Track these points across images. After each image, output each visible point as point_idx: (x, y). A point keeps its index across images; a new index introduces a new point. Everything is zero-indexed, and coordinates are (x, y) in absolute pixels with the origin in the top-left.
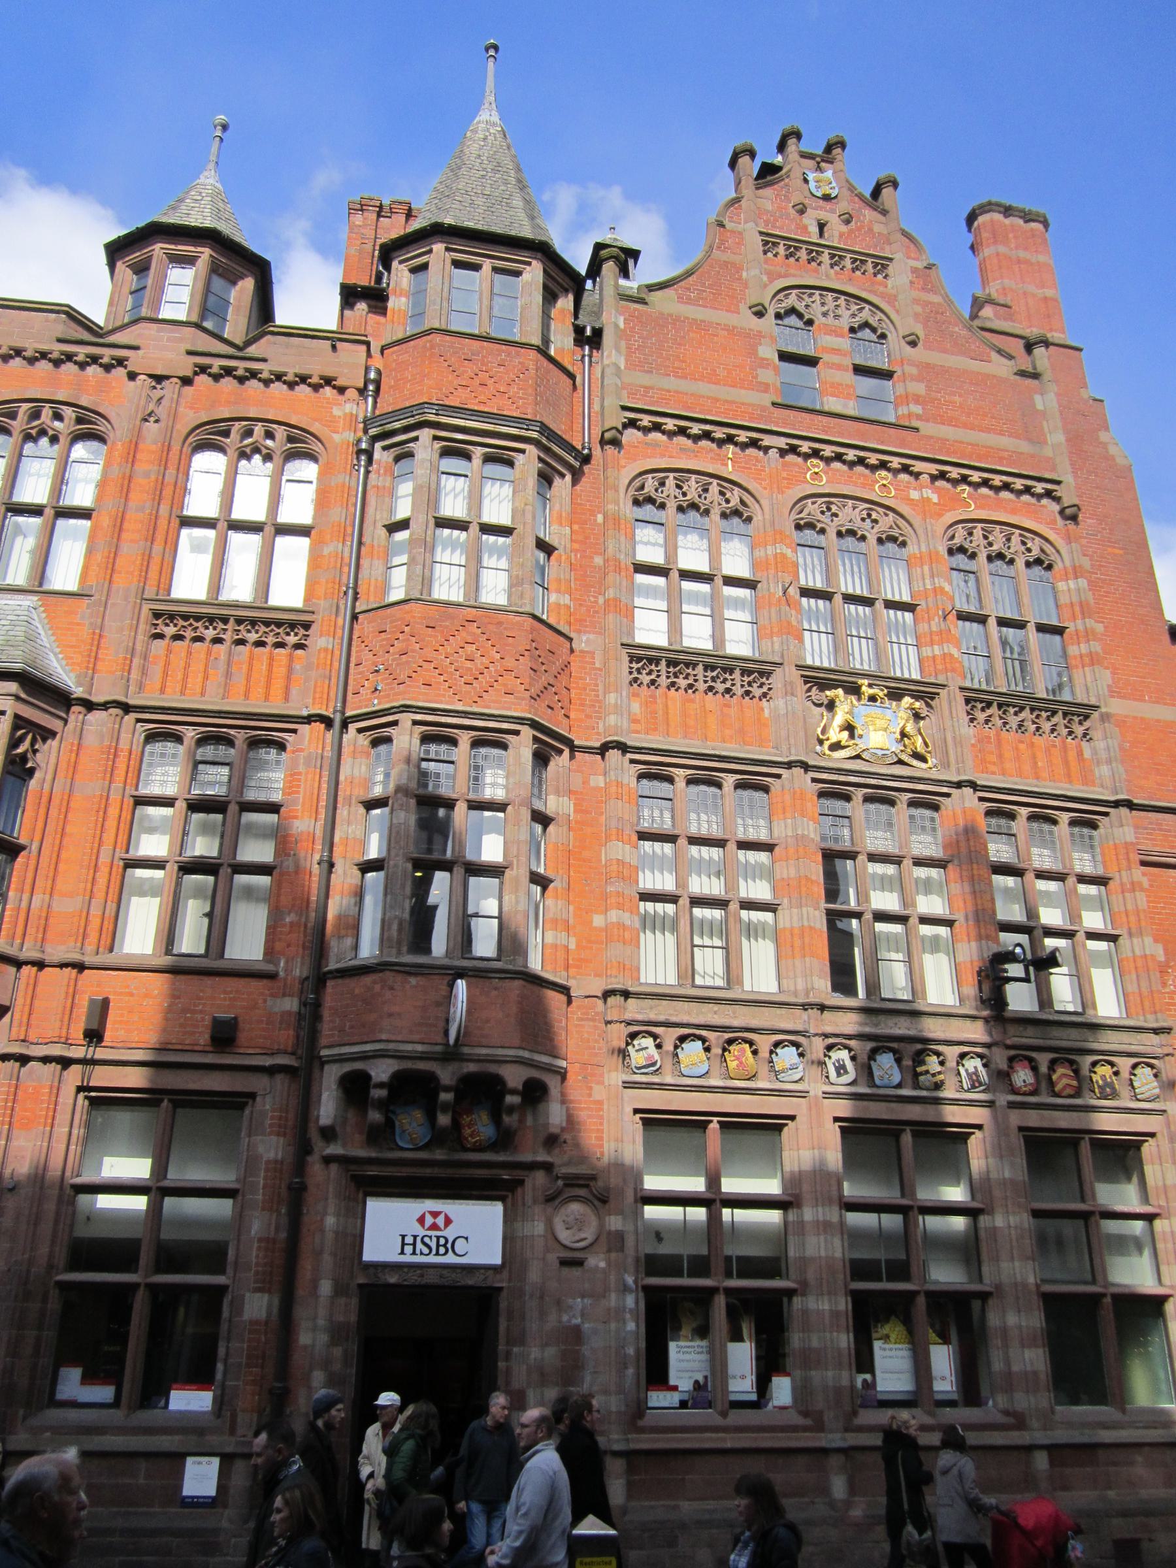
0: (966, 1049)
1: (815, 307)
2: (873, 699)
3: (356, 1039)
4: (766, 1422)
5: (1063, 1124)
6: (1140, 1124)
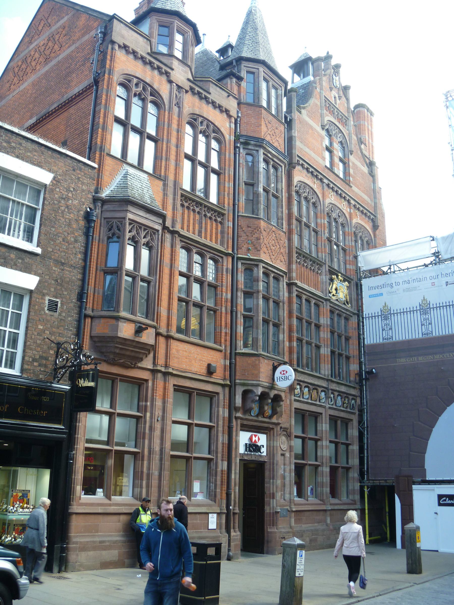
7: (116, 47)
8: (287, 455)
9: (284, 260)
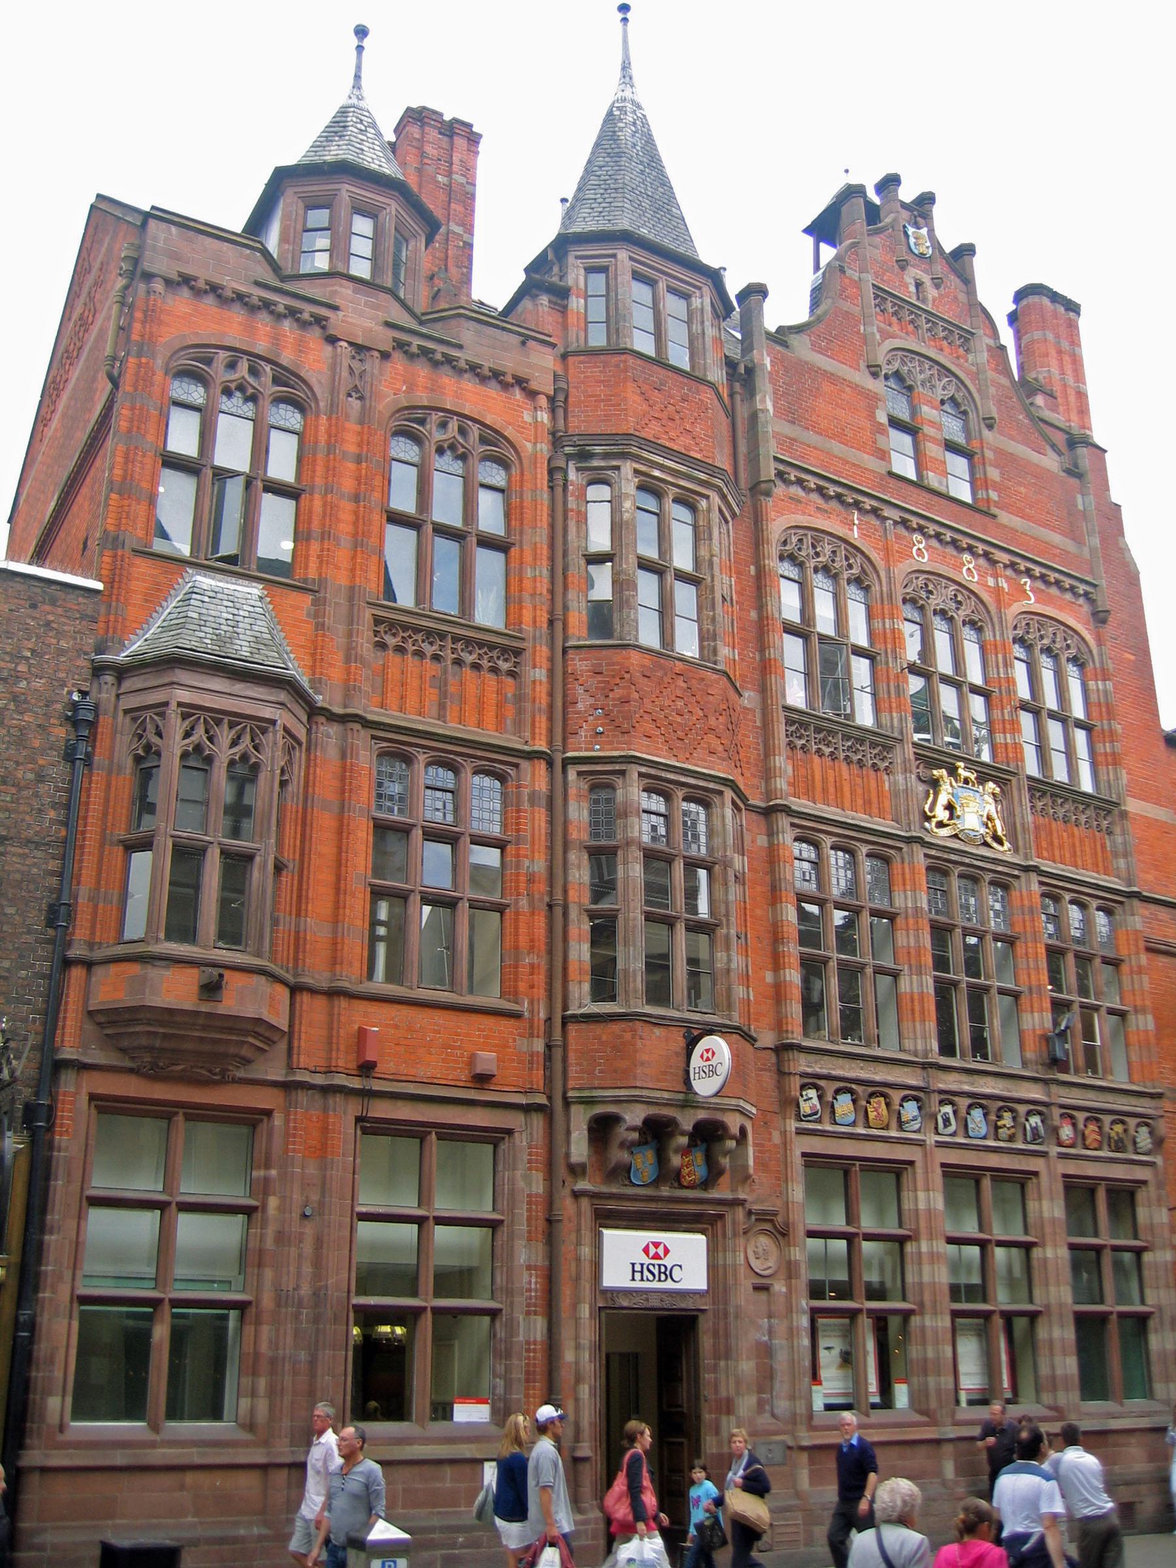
0: (1032, 1107)
1: (918, 374)
2: (966, 781)
3: (609, 1083)
4: (899, 1420)
5: (1090, 1173)
6: (1140, 1173)
7: (158, 286)
8: (779, 1287)
9: (721, 748)
